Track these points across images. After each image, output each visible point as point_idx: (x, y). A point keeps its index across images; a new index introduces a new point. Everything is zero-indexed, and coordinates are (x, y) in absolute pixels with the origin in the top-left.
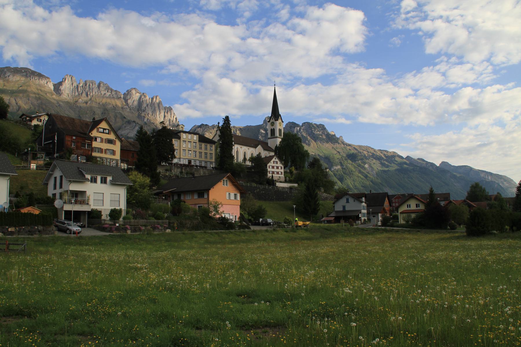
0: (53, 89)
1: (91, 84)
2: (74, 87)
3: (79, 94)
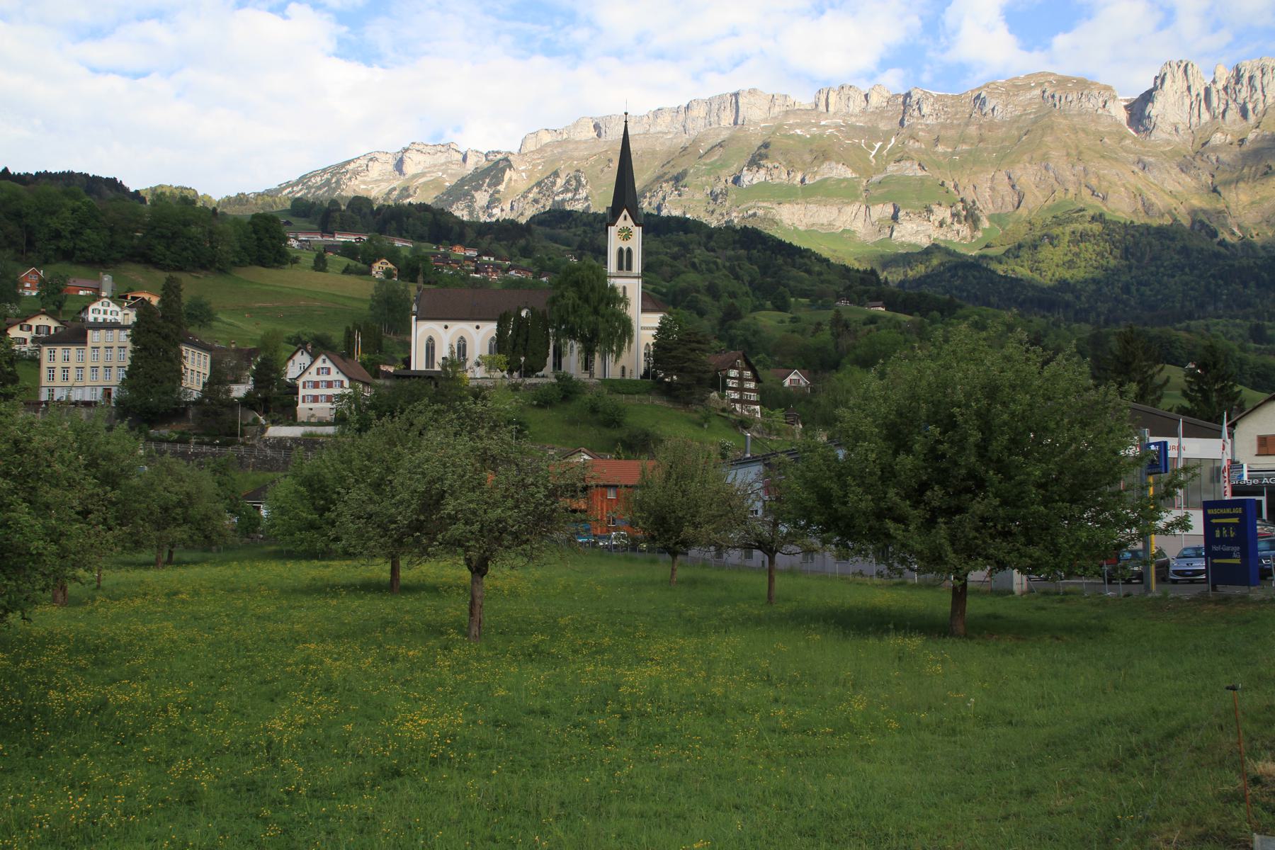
0: (1124, 122)
1: (1258, 74)
2: (1193, 99)
3: (1214, 117)
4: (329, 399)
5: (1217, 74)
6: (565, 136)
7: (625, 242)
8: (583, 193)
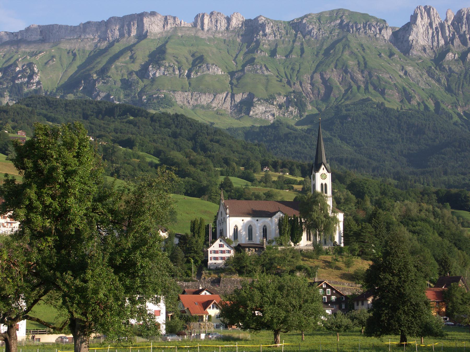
4: (222, 258)
5: (448, 16)
6: (19, 38)
7: (324, 180)
8: (36, 79)
